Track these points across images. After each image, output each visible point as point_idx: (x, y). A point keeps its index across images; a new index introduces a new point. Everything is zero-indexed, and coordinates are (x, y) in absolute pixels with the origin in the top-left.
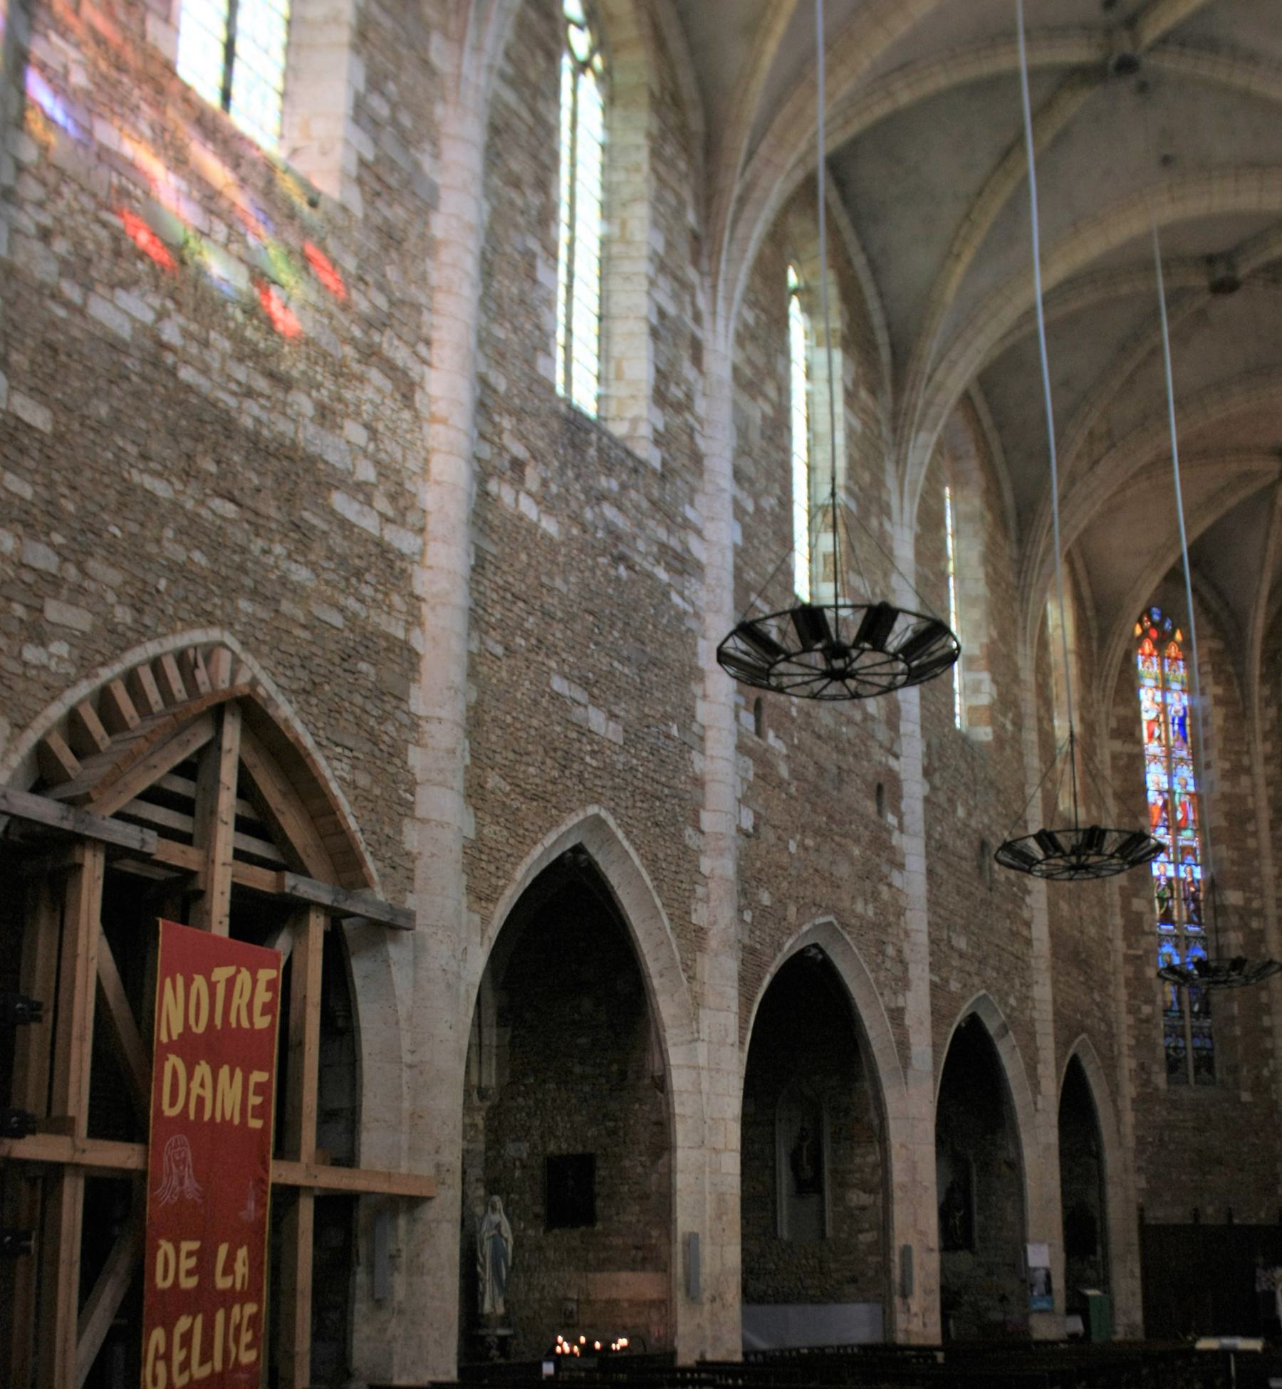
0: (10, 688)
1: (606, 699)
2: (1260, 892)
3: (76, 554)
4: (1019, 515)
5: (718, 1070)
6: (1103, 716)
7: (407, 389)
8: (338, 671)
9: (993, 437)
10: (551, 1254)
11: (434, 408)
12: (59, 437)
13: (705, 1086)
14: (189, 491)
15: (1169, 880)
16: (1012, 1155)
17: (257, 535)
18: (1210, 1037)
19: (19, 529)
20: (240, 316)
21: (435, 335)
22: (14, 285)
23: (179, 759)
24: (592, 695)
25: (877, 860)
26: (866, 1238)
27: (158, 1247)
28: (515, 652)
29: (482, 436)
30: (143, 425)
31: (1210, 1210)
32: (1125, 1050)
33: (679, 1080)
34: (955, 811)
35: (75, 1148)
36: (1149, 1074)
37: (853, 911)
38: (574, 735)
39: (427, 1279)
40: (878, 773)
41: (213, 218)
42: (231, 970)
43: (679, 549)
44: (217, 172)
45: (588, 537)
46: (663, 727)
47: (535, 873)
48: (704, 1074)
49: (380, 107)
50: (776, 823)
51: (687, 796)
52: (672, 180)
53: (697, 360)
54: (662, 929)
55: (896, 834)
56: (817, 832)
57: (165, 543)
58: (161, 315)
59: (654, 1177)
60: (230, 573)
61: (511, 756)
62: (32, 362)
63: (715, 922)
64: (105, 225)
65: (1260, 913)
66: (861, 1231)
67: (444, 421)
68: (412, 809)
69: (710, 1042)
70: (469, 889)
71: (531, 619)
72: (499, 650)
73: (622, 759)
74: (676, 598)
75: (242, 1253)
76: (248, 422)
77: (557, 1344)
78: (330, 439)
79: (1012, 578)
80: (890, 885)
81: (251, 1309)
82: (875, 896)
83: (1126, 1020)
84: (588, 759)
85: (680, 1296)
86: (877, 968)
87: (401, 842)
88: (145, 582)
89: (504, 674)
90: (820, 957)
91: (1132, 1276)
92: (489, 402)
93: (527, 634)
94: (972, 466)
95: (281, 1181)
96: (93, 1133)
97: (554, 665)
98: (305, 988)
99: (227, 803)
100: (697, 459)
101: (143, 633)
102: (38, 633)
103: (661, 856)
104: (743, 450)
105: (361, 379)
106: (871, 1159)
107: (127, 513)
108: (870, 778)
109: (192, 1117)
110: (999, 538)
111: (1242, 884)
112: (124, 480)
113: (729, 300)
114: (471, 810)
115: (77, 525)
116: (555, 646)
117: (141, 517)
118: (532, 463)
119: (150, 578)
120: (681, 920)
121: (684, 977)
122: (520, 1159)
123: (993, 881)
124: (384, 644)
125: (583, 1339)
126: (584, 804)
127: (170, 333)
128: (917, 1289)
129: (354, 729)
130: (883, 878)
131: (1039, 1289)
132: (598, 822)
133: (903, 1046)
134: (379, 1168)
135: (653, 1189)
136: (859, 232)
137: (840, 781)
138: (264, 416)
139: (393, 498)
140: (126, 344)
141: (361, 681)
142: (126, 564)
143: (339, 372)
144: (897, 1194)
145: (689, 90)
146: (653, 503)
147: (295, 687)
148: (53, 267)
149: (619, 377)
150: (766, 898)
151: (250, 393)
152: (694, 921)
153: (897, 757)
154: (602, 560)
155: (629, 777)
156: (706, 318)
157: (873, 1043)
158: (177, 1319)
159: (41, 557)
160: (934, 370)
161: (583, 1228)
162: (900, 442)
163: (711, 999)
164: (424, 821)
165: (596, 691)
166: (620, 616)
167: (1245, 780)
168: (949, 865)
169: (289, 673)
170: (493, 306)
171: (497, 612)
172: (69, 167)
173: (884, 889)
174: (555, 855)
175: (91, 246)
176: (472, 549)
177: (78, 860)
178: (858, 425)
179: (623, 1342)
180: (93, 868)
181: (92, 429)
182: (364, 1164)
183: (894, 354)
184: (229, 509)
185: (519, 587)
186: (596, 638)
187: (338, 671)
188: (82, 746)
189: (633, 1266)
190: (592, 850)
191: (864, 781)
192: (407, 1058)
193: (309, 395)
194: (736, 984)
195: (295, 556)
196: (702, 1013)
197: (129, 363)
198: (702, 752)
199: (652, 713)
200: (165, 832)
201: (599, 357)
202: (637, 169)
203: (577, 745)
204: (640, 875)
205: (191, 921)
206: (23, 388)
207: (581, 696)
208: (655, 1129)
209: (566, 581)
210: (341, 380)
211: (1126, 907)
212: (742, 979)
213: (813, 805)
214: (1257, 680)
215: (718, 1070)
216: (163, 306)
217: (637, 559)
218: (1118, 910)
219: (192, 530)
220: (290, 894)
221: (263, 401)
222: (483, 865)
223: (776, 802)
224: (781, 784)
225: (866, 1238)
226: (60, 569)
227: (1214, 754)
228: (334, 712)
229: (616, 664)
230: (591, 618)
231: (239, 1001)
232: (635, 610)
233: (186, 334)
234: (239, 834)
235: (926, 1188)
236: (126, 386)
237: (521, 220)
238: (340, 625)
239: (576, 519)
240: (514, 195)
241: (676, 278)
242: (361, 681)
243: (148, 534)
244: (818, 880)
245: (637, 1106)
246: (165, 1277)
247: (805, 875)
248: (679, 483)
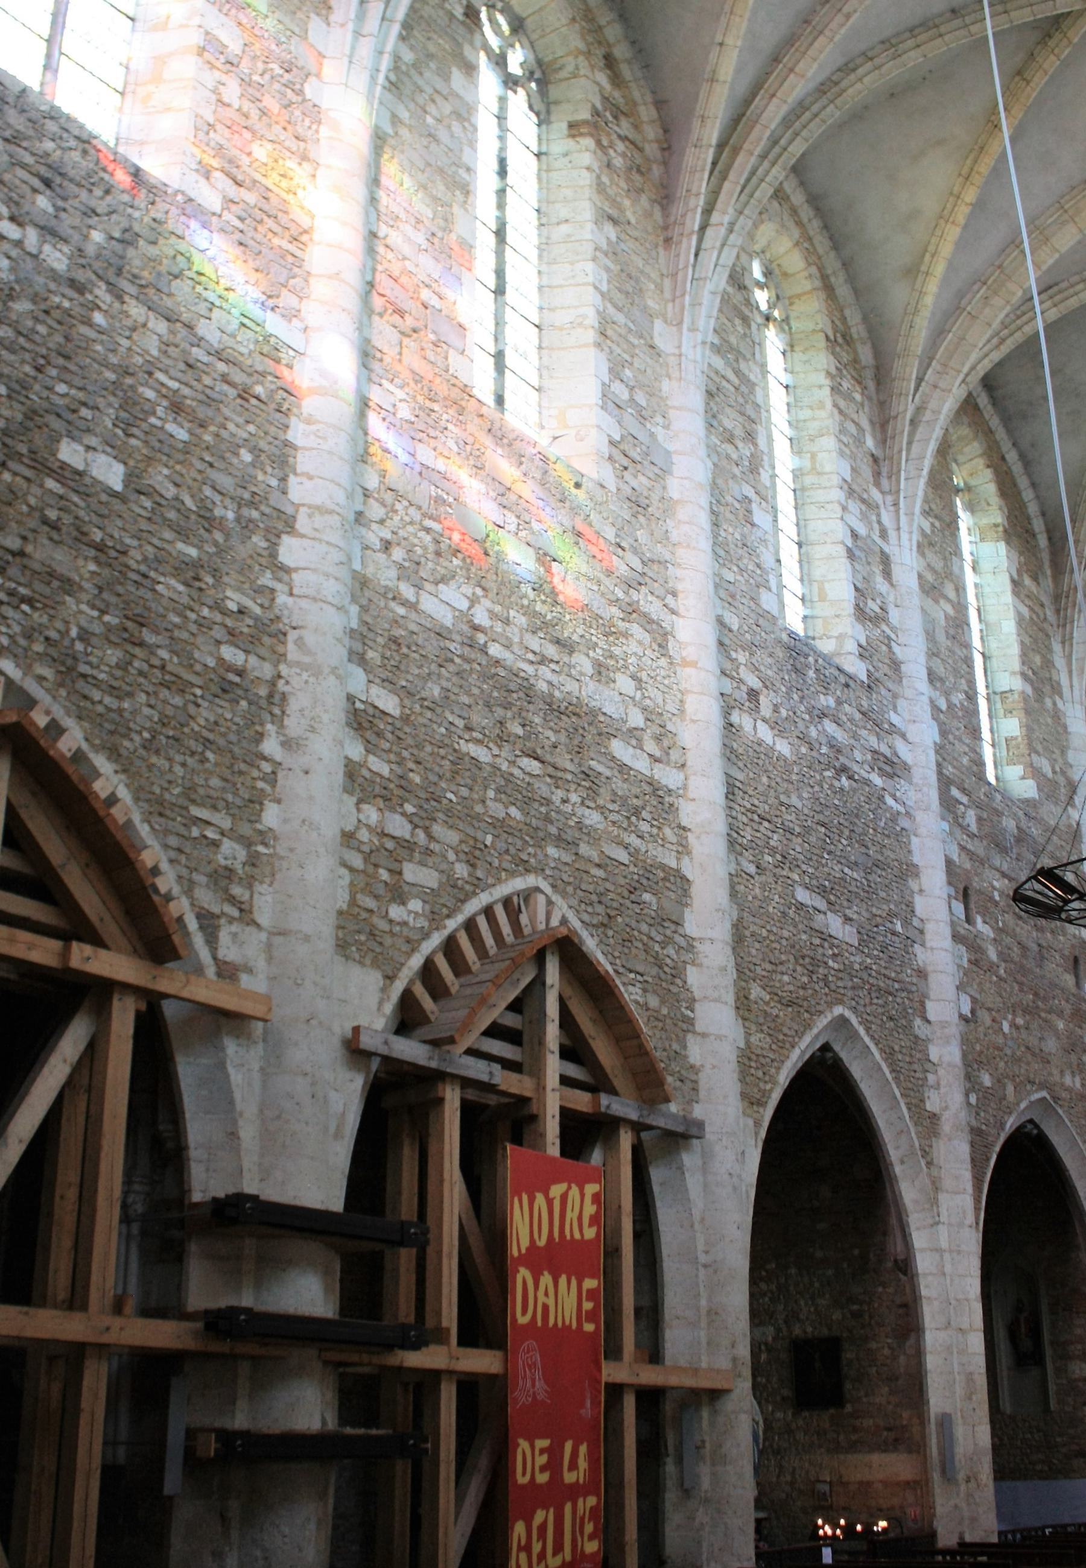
0: (381, 944)
1: (841, 905)
3: (422, 821)
5: (959, 1252)
7: (662, 638)
8: (628, 903)
10: (800, 1436)
12: (406, 719)
13: (948, 1268)
14: (503, 754)
17: (557, 787)
19: (380, 802)
20: (531, 594)
21: (680, 587)
22: (367, 593)
23: (511, 997)
24: (829, 903)
27: (518, 1445)
28: (765, 869)
30: (465, 699)
33: (923, 1263)
37: (1062, 1085)
39: (729, 1468)
40: (1073, 946)
41: (506, 512)
44: (508, 470)
45: (814, 754)
46: (889, 925)
47: (793, 1073)
48: (947, 1256)
49: (620, 391)
50: (991, 1006)
51: (914, 989)
52: (851, 411)
53: (887, 574)
54: (901, 1118)
56: (1026, 1011)
57: (488, 802)
58: (473, 601)
59: (902, 1359)
60: (540, 824)
61: (769, 967)
62: (383, 657)
63: (946, 1108)
64: (428, 530)
67: (694, 664)
68: (693, 1025)
69: (950, 1224)
70: (744, 1096)
71: (776, 837)
72: (752, 869)
73: (858, 959)
74: (890, 801)
75: (583, 1449)
76: (543, 686)
77: (819, 1528)
78: (607, 692)
81: (592, 1501)
84: (831, 963)
85: (936, 1476)
87: (686, 1057)
88: (476, 840)
89: (757, 891)
90: (1035, 1132)
92: (727, 641)
93: (773, 851)
95: (611, 1380)
96: (462, 1343)
97: (797, 878)
98: (619, 1197)
99: (553, 1032)
100: (896, 665)
101: (478, 885)
102: (398, 894)
103: (897, 1048)
105: (626, 635)
107: (459, 780)
108: (1066, 953)
109: (539, 1324)
112: (455, 750)
114: (740, 1021)
115: (423, 795)
116: (796, 860)
117: (469, 781)
118: (765, 691)
119: (479, 835)
120: (917, 1107)
121: (923, 1163)
122: (766, 1344)
124: (662, 875)
125: (842, 1522)
126: (830, 1005)
127: (481, 617)
129: (642, 955)
132: (843, 1021)
135: (902, 1370)
136: (1009, 432)
138: (554, 679)
139: (658, 739)
140: (450, 631)
141: (646, 911)
145: (858, 330)
147: (595, 922)
148: (393, 573)
149: (823, 598)
150: (987, 1080)
151: (543, 660)
152: (928, 1108)
154: (827, 774)
155: (865, 977)
156: (892, 534)
158: (534, 1512)
159: (398, 826)
161: (832, 1411)
163: (947, 1183)
164: (704, 1035)
165: (832, 898)
166: (846, 824)
169: (590, 909)
170: (722, 553)
171: (748, 833)
172: (400, 487)
175: (419, 551)
177: (440, 1094)
178: (1025, 611)
179: (883, 1524)
180: (452, 1098)
181: (428, 708)
182: (668, 1360)
184: (534, 766)
185: (763, 808)
186: (828, 847)
187: (628, 903)
189: (885, 1447)
190: (837, 1047)
191: (1062, 956)
192: (703, 1258)
193: (588, 655)
194: (969, 1167)
195: (588, 803)
196: (942, 1197)
198: (923, 945)
199: (879, 912)
201: (802, 580)
202: (821, 405)
203: (820, 950)
204: (880, 1069)
205: (525, 1142)
206: (377, 681)
207: (821, 904)
208: (901, 1311)
209: (800, 797)
210: (611, 639)
213: (1021, 984)
216: (474, 594)
217: (855, 767)
221: (553, 666)
222: (753, 1071)
223: (988, 985)
224: (992, 968)
226: (412, 835)
228: (627, 941)
229: (846, 870)
230: (823, 830)
231: (571, 1215)
233: (493, 615)
234: (564, 1062)
237: (736, 471)
238: (627, 862)
239: (803, 738)
241: (863, 501)
242: (646, 911)
243: (476, 796)
244: (1029, 1057)
246: (524, 1474)
247: (1018, 1053)
248: (883, 692)
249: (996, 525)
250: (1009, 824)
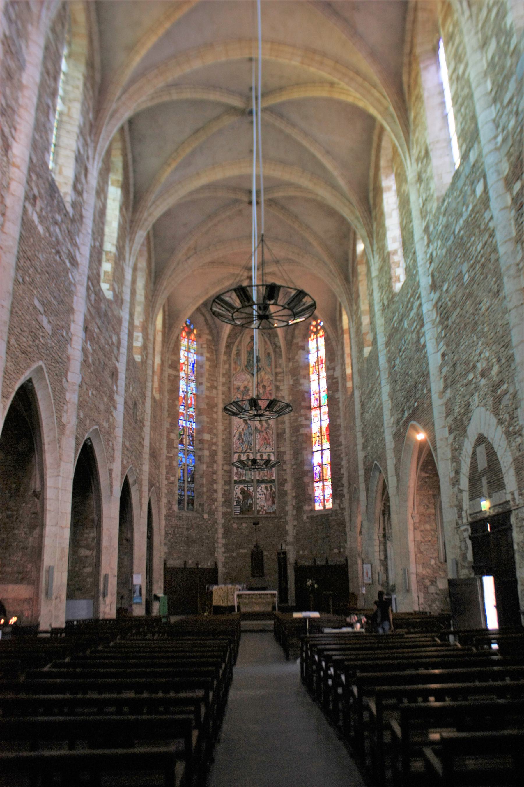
2: (216, 435)
6: (167, 358)
13: (60, 498)
15: (183, 427)
16: (129, 536)
18: (193, 491)
21: (18, 127)
26: (88, 570)
31: (190, 561)
32: (164, 495)
36: (172, 505)
48: (60, 491)
53: (86, 176)
54: (53, 423)
56: (97, 389)
59: (31, 539)
61: (20, 331)
63: (69, 423)
65: (215, 444)
66: (84, 567)
67: (18, 167)
79: (150, 298)
80: (112, 416)
83: (165, 482)
85: (43, 596)
91: (160, 588)
93: (29, 276)
100: (82, 217)
106: (92, 535)
111: (210, 432)
130: (111, 412)
131: (137, 594)
133: (111, 486)
135: (30, 544)
136: (132, 145)
144: (104, 551)
153: (118, 362)
160: (150, 206)
167: (214, 391)
173: (111, 417)
183: (135, 197)
189: (17, 582)
190: (34, 381)
196: (62, 464)
198: (71, 345)
202: (78, 88)
208: (33, 516)
211: (168, 436)
214: (223, 353)
215: (65, 490)
218: (165, 437)
225: (88, 570)
227: (204, 380)
237: (48, 90)
239: (48, 229)
245: (24, 505)
249: (118, 181)
250: (103, 306)
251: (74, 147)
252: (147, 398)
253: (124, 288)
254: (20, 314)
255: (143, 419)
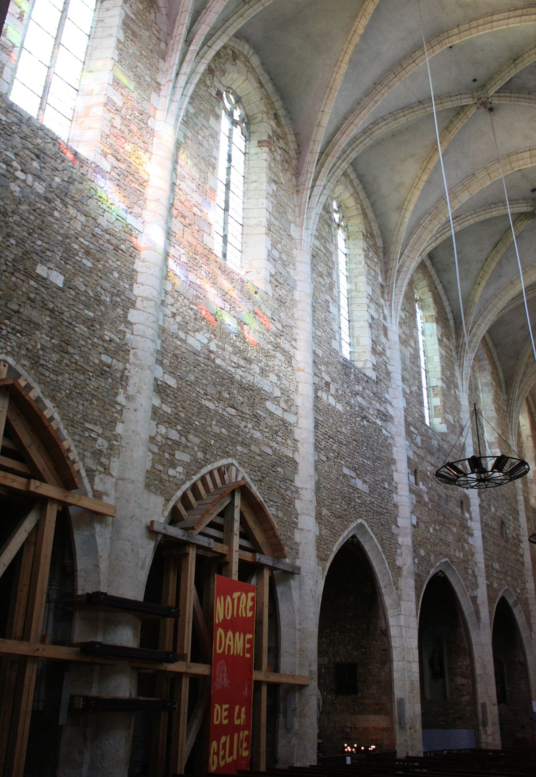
3: (184, 433)
4: (506, 382)
5: (409, 627)
7: (289, 359)
9: (493, 350)
11: (299, 366)
12: (179, 389)
13: (404, 634)
20: (235, 338)
21: (298, 337)
22: (165, 335)
25: (463, 533)
26: (466, 698)
29: (315, 374)
33: (393, 632)
34: (490, 509)
35: (187, 666)
38: (352, 491)
42: (239, 593)
43: (384, 411)
44: (227, 285)
45: (352, 410)
47: (339, 547)
48: (403, 628)
53: (386, 335)
54: (385, 568)
55: (469, 521)
56: (440, 524)
57: (213, 426)
58: (210, 340)
61: (330, 501)
63: (405, 564)
64: (192, 309)
66: (462, 696)
67: (303, 370)
70: (318, 556)
71: (335, 445)
74: (384, 432)
75: (243, 709)
78: (265, 381)
79: (505, 408)
80: (468, 543)
81: (246, 733)
82: (463, 548)
84: (357, 500)
85: (397, 726)
86: (465, 579)
87: (294, 539)
89: (326, 468)
92: (317, 361)
93: (334, 451)
94: (486, 363)
95: (256, 679)
97: (343, 463)
99: (237, 526)
100: (388, 374)
101: (207, 462)
104: (404, 369)
105: (274, 357)
106: (465, 663)
108: (458, 499)
109: (226, 653)
110: (499, 392)
113: (396, 310)
119: (208, 440)
121: (394, 588)
123: (507, 538)
126: (356, 518)
127: (213, 347)
128: (490, 724)
129: (276, 494)
130: (466, 541)
133: (477, 613)
134: (288, 673)
136: (439, 276)
137: (447, 501)
138: (243, 374)
139: (286, 402)
140: (199, 353)
142: (201, 436)
143: (267, 355)
144: (478, 679)
145: (376, 231)
146: (374, 394)
148: (176, 327)
149: (358, 344)
150: (422, 553)
154: (358, 419)
155: (372, 507)
156: (388, 318)
157: (465, 612)
159: (174, 435)
160: (472, 329)
162: (460, 358)
163: (405, 597)
164: (302, 530)
168: (490, 533)
169: (255, 474)
170: (316, 323)
171: (323, 443)
172: (180, 290)
173: (466, 545)
174: (346, 540)
175: (188, 318)
176: (314, 419)
178: (444, 353)
179: (373, 747)
180: (192, 553)
184: (233, 411)
188: (188, 506)
190: (358, 537)
191: (456, 500)
192: (298, 627)
195: (255, 428)
197: (200, 359)
198: (397, 494)
200: (217, 540)
202: (360, 263)
203: (353, 495)
204: (377, 547)
207: (353, 474)
208: (383, 652)
209: (346, 429)
212: (416, 587)
213: (438, 512)
217: (370, 417)
219: (223, 421)
220: (258, 563)
221: (243, 369)
224: (426, 504)
225: (466, 698)
231: (242, 606)
232: (370, 437)
235: (490, 676)
236: (199, 368)
237: (323, 289)
239: (348, 403)
240: (320, 279)
241: (377, 304)
248: (383, 385)
250: (435, 443)
251: (367, 317)
252: (520, 513)
253: (462, 415)
254: (329, 487)
255: (518, 535)
